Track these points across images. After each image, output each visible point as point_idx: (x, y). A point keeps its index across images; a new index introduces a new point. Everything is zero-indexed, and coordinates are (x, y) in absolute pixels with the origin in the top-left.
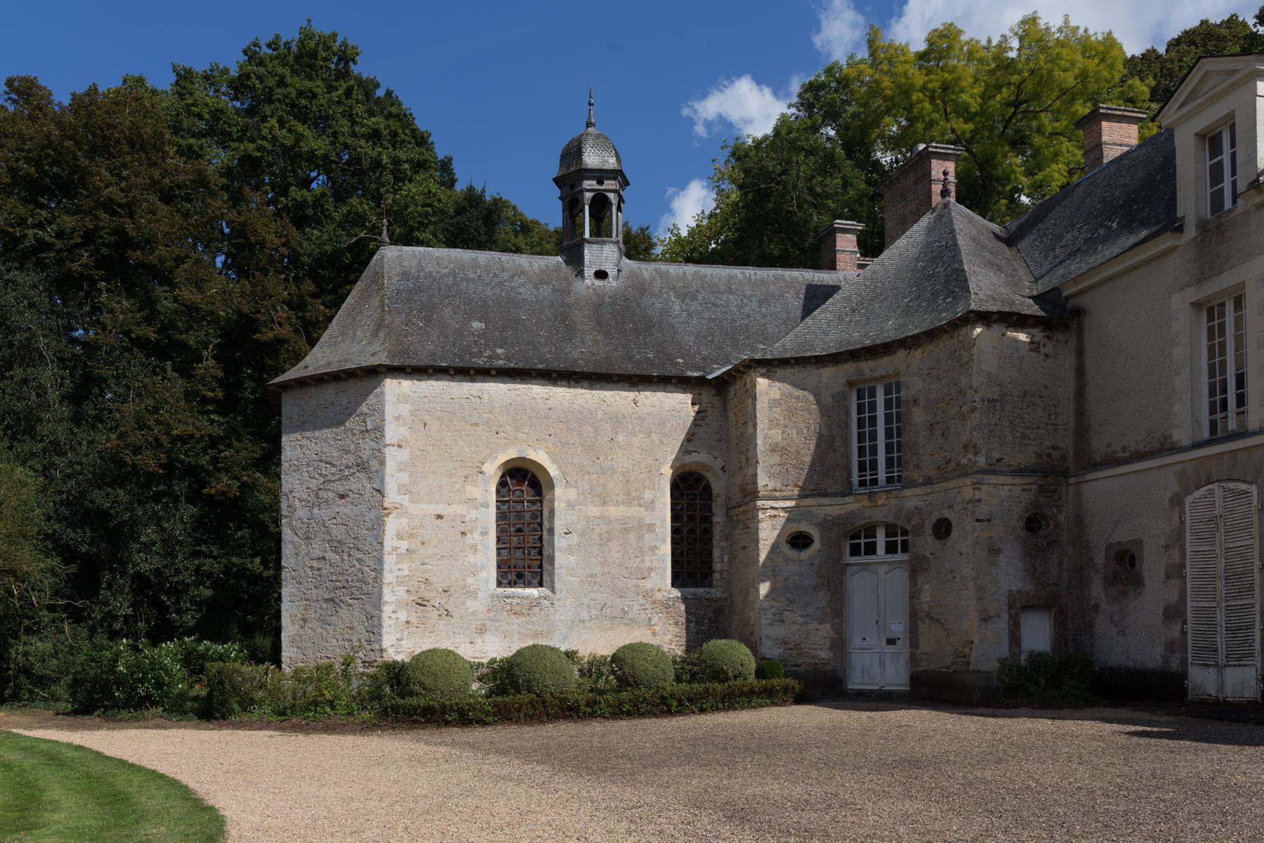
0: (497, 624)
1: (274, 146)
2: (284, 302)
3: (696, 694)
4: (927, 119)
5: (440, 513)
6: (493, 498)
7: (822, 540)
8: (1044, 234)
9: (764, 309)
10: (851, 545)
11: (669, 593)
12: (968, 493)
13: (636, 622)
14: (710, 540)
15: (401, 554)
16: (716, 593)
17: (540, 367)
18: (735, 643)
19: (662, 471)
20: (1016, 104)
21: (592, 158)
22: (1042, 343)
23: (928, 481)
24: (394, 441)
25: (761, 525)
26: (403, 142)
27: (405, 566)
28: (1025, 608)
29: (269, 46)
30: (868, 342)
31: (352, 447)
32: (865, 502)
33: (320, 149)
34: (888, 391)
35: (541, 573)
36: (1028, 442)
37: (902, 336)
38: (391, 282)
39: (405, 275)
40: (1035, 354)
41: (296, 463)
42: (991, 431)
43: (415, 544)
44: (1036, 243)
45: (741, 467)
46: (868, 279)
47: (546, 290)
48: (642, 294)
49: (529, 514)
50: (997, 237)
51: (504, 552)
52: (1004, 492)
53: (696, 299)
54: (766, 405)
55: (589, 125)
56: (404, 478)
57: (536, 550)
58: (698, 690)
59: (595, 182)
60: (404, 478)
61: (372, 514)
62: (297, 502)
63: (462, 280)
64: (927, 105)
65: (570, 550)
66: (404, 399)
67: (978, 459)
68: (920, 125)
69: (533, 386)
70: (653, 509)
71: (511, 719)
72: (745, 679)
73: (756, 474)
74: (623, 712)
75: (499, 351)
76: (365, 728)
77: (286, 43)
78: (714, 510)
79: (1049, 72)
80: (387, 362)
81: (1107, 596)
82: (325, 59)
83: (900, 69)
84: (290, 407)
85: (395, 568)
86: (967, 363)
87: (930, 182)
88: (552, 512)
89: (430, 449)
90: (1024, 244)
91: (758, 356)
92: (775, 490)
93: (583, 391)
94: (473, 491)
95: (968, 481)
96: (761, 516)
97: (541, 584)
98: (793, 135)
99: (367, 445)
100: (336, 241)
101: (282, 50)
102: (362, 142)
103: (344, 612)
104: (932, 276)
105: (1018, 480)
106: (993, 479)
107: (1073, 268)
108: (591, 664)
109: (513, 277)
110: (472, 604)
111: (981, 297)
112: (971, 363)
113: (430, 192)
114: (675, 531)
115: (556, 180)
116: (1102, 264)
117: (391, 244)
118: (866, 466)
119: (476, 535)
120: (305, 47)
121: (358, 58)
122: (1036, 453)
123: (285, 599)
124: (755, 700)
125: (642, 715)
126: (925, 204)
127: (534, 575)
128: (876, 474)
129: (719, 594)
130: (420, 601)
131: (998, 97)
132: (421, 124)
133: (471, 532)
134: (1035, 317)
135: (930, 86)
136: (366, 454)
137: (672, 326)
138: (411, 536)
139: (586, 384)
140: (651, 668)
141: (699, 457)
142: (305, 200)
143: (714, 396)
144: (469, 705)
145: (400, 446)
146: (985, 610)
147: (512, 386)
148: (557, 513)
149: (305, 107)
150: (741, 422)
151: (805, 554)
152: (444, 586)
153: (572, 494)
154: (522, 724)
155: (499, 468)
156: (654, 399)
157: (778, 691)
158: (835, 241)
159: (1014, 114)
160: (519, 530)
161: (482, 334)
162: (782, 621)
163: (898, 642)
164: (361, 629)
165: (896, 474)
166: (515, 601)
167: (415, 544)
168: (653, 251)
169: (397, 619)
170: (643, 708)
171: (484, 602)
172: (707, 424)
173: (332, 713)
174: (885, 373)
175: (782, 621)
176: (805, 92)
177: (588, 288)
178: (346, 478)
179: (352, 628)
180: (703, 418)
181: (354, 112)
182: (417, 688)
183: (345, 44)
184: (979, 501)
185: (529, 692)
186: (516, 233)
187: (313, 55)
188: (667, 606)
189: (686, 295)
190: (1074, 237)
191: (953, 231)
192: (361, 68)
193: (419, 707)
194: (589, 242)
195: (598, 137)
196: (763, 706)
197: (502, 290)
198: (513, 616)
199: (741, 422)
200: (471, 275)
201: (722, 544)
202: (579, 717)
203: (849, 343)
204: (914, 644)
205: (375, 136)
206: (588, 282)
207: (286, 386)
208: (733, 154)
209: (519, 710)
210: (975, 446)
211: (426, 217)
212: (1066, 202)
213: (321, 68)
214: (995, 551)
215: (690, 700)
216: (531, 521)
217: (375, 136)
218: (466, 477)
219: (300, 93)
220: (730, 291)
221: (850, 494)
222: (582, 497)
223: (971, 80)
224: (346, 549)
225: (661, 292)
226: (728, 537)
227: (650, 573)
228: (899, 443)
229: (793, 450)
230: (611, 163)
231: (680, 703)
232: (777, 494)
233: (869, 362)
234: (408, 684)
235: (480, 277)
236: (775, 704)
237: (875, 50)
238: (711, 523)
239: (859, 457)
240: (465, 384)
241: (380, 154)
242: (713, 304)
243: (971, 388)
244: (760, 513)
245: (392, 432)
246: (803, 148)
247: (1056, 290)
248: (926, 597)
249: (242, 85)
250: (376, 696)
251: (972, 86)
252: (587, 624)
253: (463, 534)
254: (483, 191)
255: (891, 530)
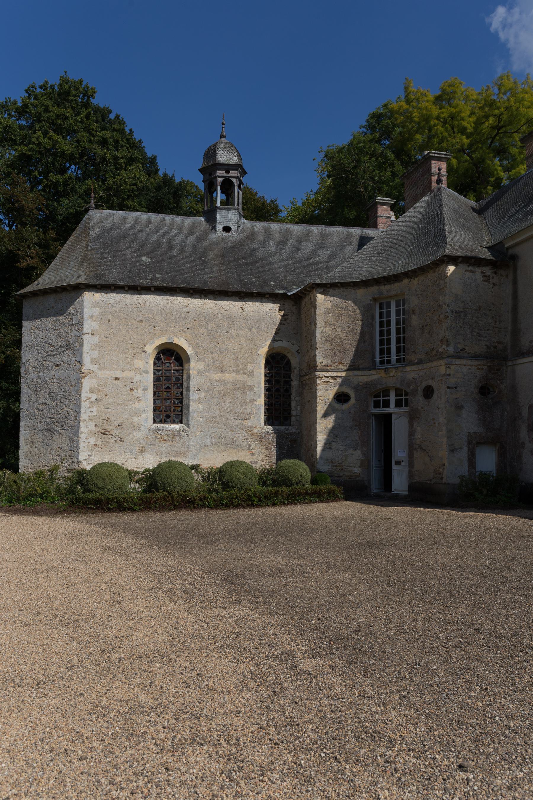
0: (152, 447)
1: (40, 148)
2: (36, 244)
3: (270, 494)
4: (440, 136)
5: (117, 376)
6: (151, 367)
7: (356, 397)
8: (500, 208)
9: (329, 252)
10: (374, 401)
11: (263, 429)
12: (443, 370)
13: (241, 447)
14: (290, 396)
15: (92, 402)
16: (292, 429)
17: (182, 286)
18: (298, 462)
19: (259, 352)
20: (497, 128)
21: (222, 157)
22: (491, 276)
23: (420, 362)
24: (89, 331)
25: (318, 388)
26: (122, 146)
27: (94, 409)
28: (479, 444)
29: (41, 87)
30: (385, 274)
31: (64, 334)
32: (383, 374)
33: (68, 150)
34: (398, 305)
35: (182, 415)
36: (482, 338)
37: (405, 270)
38: (94, 232)
39: (103, 228)
40: (486, 283)
41: (30, 344)
42: (458, 331)
43: (101, 395)
44: (495, 214)
45: (308, 350)
46: (389, 235)
47: (192, 238)
48: (252, 241)
49: (174, 378)
50: (474, 209)
51: (159, 402)
52: (465, 370)
53: (287, 245)
54: (322, 312)
55: (222, 136)
56: (95, 354)
57: (179, 401)
58: (271, 492)
59: (224, 172)
60: (95, 354)
61: (75, 376)
62: (30, 368)
63: (139, 231)
64: (440, 127)
65: (199, 401)
66: (96, 305)
67: (448, 349)
68: (436, 140)
69: (178, 298)
70: (253, 376)
71: (150, 508)
72: (304, 485)
73: (316, 355)
74: (222, 505)
75: (158, 276)
76: (59, 512)
77: (52, 86)
78: (292, 377)
79: (517, 109)
80: (86, 282)
81: (529, 437)
82: (75, 96)
83: (423, 105)
84: (27, 308)
85: (88, 411)
86: (443, 288)
87: (431, 174)
88: (189, 377)
89: (112, 336)
90: (488, 213)
91: (318, 281)
92: (327, 366)
93: (210, 301)
94: (139, 363)
95: (442, 362)
96: (318, 381)
97: (181, 422)
98: (362, 145)
99: (73, 333)
100: (78, 207)
101: (49, 90)
102: (96, 146)
103: (57, 437)
104: (427, 233)
105: (475, 363)
106: (458, 362)
107: (513, 230)
108: (209, 474)
109: (171, 229)
110: (136, 434)
111: (454, 246)
112: (445, 288)
113: (135, 176)
114: (267, 390)
115: (200, 170)
116: (528, 227)
117: (96, 209)
118: (385, 351)
119: (140, 391)
120: (62, 88)
121: (95, 95)
122: (487, 346)
123: (22, 429)
124: (308, 498)
125: (235, 507)
126: (428, 188)
127: (177, 416)
128: (390, 357)
129: (294, 430)
130: (103, 432)
131: (487, 123)
132: (137, 137)
133: (137, 389)
134: (486, 260)
135: (442, 116)
136: (72, 339)
137: (270, 261)
138: (99, 390)
139: (211, 296)
140: (243, 477)
141: (283, 344)
142: (58, 181)
143: (293, 305)
144: (124, 498)
145: (93, 334)
146: (452, 445)
147: (164, 297)
148: (192, 377)
149: (60, 124)
150: (308, 322)
151: (345, 406)
152: (119, 422)
153: (201, 366)
154: (157, 511)
155: (155, 349)
156: (255, 307)
157: (324, 493)
158: (376, 210)
159: (498, 133)
160: (168, 388)
161: (148, 265)
162: (330, 448)
163: (403, 463)
164: (66, 448)
165: (402, 357)
166: (164, 432)
167: (101, 395)
168: (279, 215)
169: (89, 443)
170: (236, 501)
171: (144, 433)
172: (288, 323)
173: (42, 501)
174: (395, 293)
175: (330, 448)
176: (371, 118)
177: (219, 237)
178: (60, 354)
179: (61, 448)
180: (285, 320)
181: (91, 128)
182: (92, 487)
183: (87, 86)
184: (449, 375)
185: (164, 491)
186: (197, 202)
187: (68, 93)
188: (261, 437)
189: (280, 242)
190: (516, 210)
191: (441, 205)
192: (98, 101)
193: (93, 499)
194: (220, 209)
195: (227, 144)
196: (313, 503)
197: (164, 238)
198: (163, 442)
199: (308, 322)
200: (145, 228)
201: (297, 399)
202: (194, 507)
203: (374, 274)
204: (411, 465)
205: (104, 143)
206: (218, 233)
207: (25, 296)
208: (326, 156)
209: (156, 503)
210: (447, 340)
211: (132, 192)
212: (514, 189)
213: (72, 100)
214: (459, 407)
215: (266, 497)
216: (176, 382)
217: (104, 143)
218: (134, 354)
219: (58, 116)
220: (308, 240)
221: (375, 369)
222: (207, 368)
223: (468, 113)
224: (59, 398)
225: (264, 240)
226: (300, 394)
227: (250, 417)
228: (404, 337)
229: (339, 340)
230: (235, 160)
231: (260, 500)
232: (328, 368)
233: (386, 286)
234: (87, 485)
235: (150, 229)
236: (321, 501)
237: (408, 94)
238: (290, 385)
239: (380, 346)
240: (135, 296)
241: (105, 154)
242: (297, 248)
243: (445, 304)
244: (318, 379)
245: (88, 325)
246: (367, 153)
247: (501, 243)
248: (418, 436)
249: (23, 111)
250: (71, 490)
251: (469, 117)
252: (210, 448)
253: (132, 390)
254: (173, 176)
255: (399, 393)
